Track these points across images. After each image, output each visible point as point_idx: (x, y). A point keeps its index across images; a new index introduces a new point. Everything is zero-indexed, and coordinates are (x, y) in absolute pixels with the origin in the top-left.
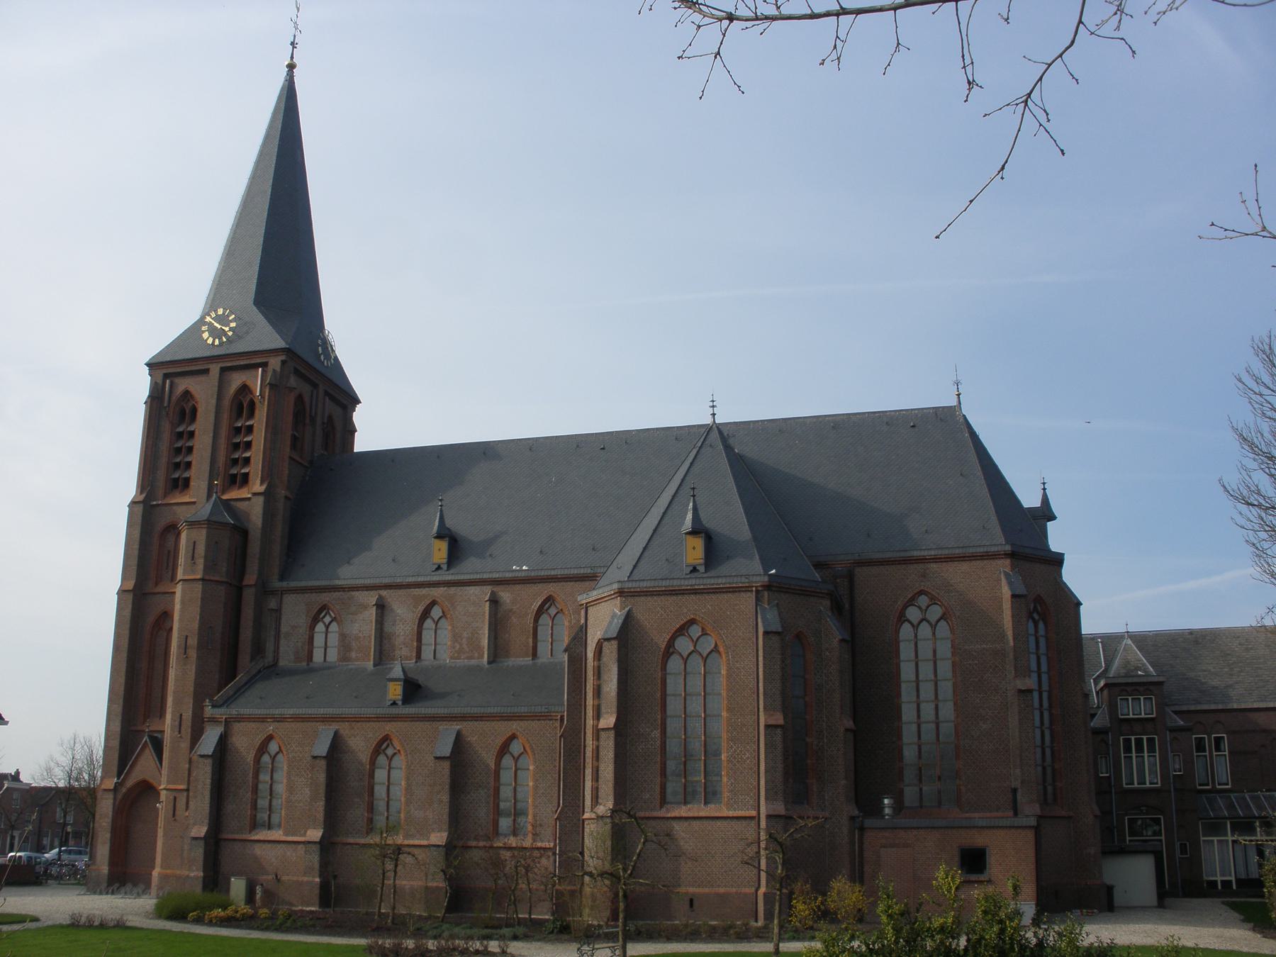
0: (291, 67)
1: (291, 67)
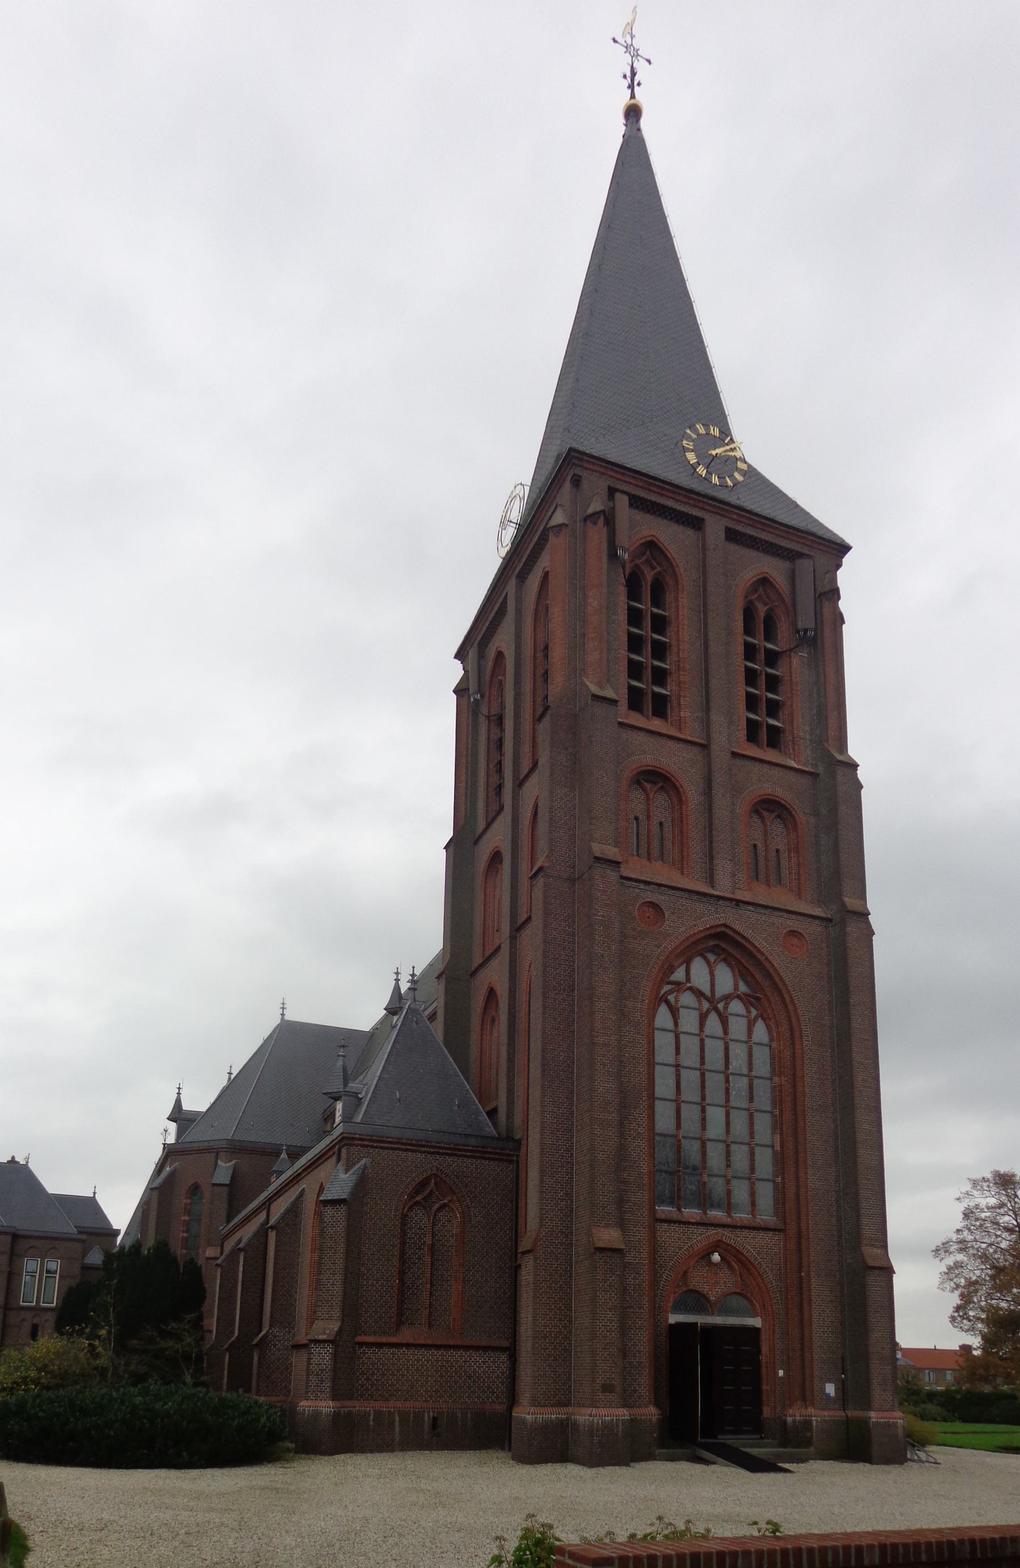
0: (633, 113)
1: (633, 113)
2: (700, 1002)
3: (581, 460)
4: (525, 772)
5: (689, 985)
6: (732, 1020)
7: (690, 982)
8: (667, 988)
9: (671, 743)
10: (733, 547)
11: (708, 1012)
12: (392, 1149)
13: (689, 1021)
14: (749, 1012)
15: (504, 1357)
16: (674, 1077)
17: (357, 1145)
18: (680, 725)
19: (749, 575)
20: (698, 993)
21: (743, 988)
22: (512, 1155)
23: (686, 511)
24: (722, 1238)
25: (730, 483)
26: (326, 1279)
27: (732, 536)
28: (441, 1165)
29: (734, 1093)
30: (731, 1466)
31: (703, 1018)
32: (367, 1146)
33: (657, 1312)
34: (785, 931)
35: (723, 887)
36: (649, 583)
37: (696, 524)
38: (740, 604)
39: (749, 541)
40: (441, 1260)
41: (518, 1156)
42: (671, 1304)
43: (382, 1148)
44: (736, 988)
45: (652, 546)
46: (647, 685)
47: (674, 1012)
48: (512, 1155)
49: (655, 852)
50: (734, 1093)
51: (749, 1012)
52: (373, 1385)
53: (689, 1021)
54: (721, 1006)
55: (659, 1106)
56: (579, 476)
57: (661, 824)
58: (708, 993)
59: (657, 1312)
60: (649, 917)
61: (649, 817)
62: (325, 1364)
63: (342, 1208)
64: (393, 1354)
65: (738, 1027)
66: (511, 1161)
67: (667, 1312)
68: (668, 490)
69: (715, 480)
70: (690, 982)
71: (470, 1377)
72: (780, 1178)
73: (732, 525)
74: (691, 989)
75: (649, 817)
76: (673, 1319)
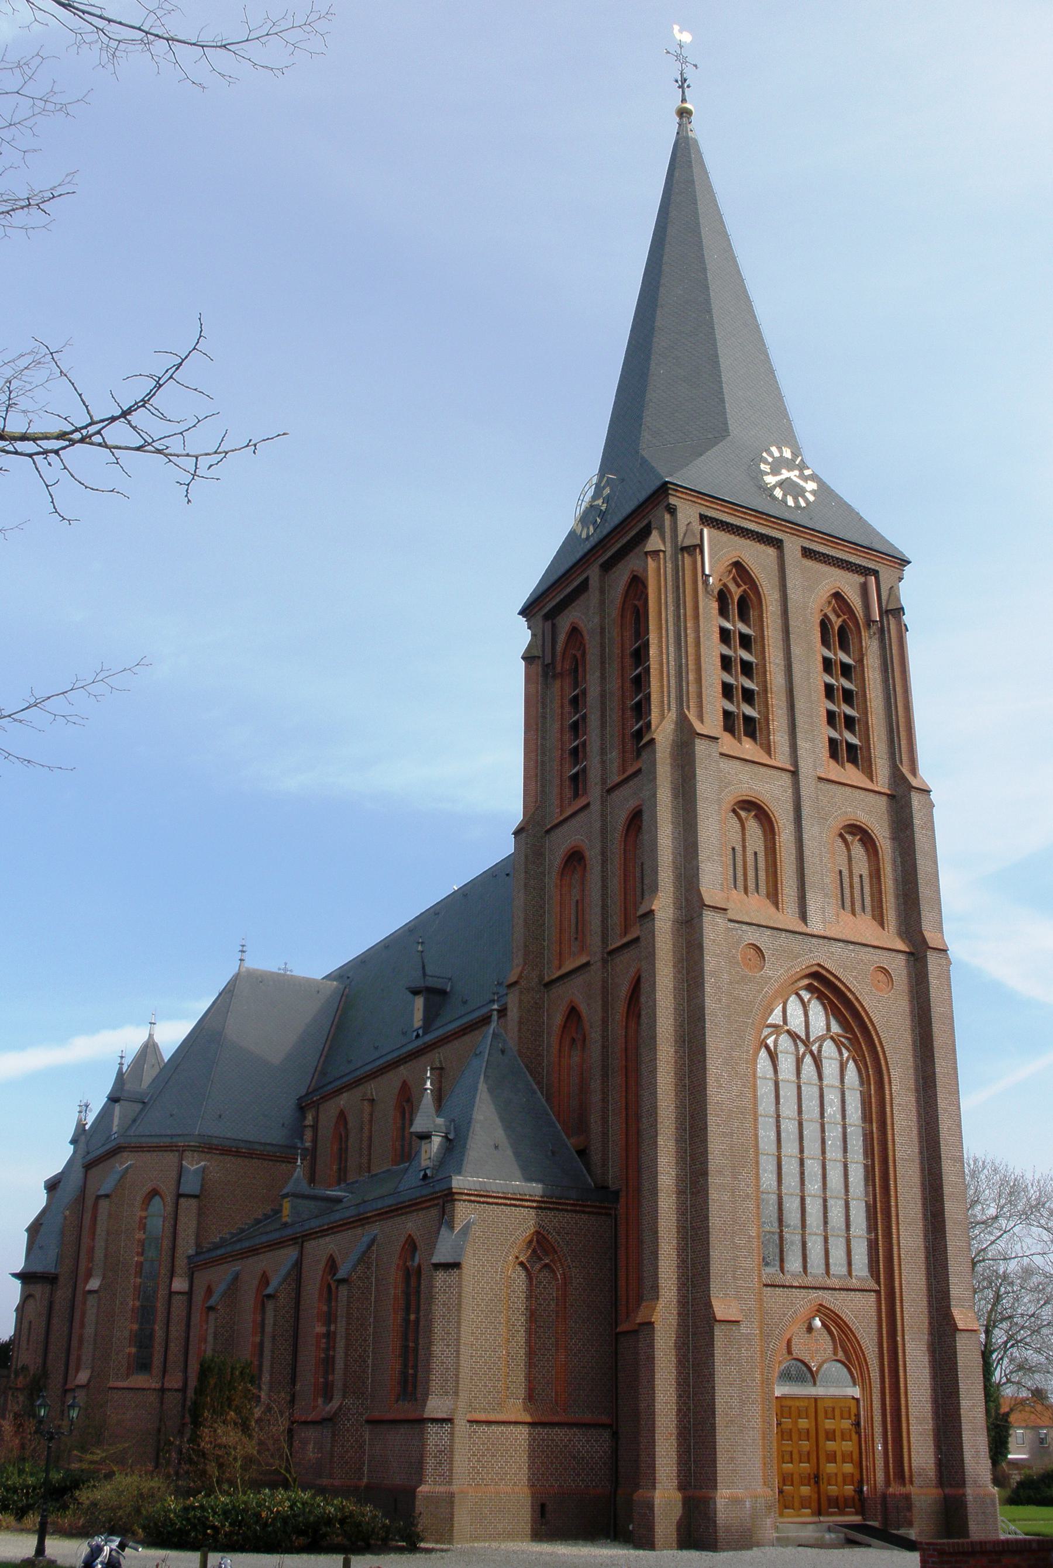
2: (796, 1045)
3: (676, 491)
4: (153, 449)
5: (786, 1028)
6: (825, 1063)
7: (787, 1025)
8: (767, 1031)
9: (763, 770)
10: (809, 563)
11: (804, 1055)
12: (497, 1204)
13: (787, 1064)
14: (841, 1054)
15: (606, 1435)
16: (774, 1128)
17: (464, 1201)
18: (768, 749)
19: (824, 591)
20: (793, 1036)
21: (835, 1028)
22: (610, 1208)
23: (767, 533)
24: (823, 1301)
25: (803, 504)
26: (440, 1351)
27: (807, 553)
28: (542, 1221)
29: (830, 1142)
30: (894, 1549)
31: (799, 1062)
32: (474, 1202)
33: (767, 1383)
34: (872, 968)
35: (816, 926)
36: (736, 601)
37: (777, 544)
38: (817, 619)
39: (822, 558)
40: (542, 1327)
41: (616, 1209)
42: (776, 1375)
43: (488, 1203)
44: (828, 1029)
45: (739, 568)
46: (738, 707)
47: (773, 1056)
48: (610, 1208)
49: (751, 885)
50: (830, 1142)
51: (841, 1054)
52: (483, 1467)
53: (787, 1064)
54: (815, 1048)
55: (763, 1159)
56: (675, 506)
57: (756, 853)
58: (803, 1036)
59: (767, 1383)
60: (750, 960)
61: (744, 847)
62: (444, 1445)
63: (455, 1272)
64: (502, 1433)
65: (830, 1068)
66: (608, 1215)
67: (774, 1385)
68: (751, 515)
69: (790, 502)
70: (787, 1025)
71: (574, 1458)
72: (873, 1234)
73: (807, 544)
74: (788, 1032)
75: (744, 847)
76: (779, 1391)
